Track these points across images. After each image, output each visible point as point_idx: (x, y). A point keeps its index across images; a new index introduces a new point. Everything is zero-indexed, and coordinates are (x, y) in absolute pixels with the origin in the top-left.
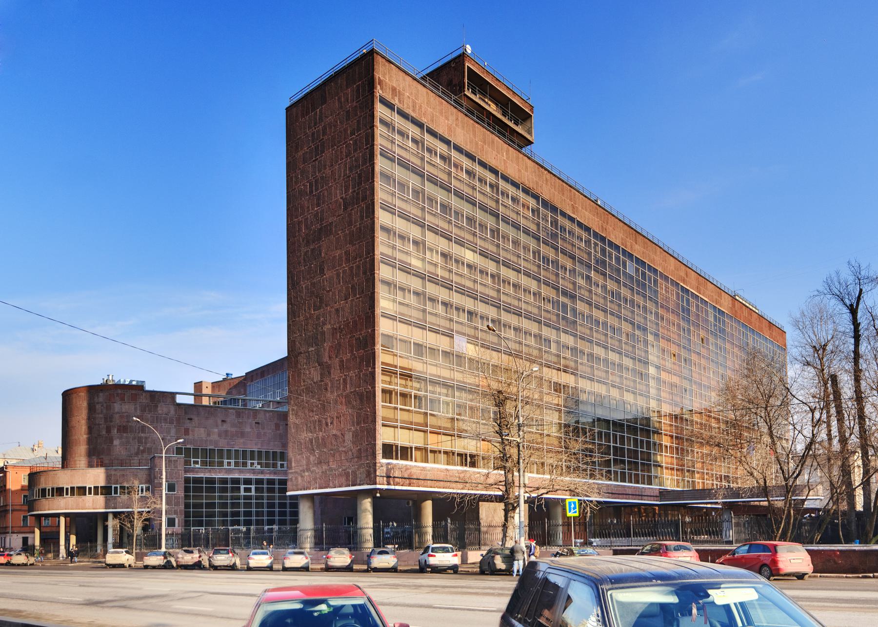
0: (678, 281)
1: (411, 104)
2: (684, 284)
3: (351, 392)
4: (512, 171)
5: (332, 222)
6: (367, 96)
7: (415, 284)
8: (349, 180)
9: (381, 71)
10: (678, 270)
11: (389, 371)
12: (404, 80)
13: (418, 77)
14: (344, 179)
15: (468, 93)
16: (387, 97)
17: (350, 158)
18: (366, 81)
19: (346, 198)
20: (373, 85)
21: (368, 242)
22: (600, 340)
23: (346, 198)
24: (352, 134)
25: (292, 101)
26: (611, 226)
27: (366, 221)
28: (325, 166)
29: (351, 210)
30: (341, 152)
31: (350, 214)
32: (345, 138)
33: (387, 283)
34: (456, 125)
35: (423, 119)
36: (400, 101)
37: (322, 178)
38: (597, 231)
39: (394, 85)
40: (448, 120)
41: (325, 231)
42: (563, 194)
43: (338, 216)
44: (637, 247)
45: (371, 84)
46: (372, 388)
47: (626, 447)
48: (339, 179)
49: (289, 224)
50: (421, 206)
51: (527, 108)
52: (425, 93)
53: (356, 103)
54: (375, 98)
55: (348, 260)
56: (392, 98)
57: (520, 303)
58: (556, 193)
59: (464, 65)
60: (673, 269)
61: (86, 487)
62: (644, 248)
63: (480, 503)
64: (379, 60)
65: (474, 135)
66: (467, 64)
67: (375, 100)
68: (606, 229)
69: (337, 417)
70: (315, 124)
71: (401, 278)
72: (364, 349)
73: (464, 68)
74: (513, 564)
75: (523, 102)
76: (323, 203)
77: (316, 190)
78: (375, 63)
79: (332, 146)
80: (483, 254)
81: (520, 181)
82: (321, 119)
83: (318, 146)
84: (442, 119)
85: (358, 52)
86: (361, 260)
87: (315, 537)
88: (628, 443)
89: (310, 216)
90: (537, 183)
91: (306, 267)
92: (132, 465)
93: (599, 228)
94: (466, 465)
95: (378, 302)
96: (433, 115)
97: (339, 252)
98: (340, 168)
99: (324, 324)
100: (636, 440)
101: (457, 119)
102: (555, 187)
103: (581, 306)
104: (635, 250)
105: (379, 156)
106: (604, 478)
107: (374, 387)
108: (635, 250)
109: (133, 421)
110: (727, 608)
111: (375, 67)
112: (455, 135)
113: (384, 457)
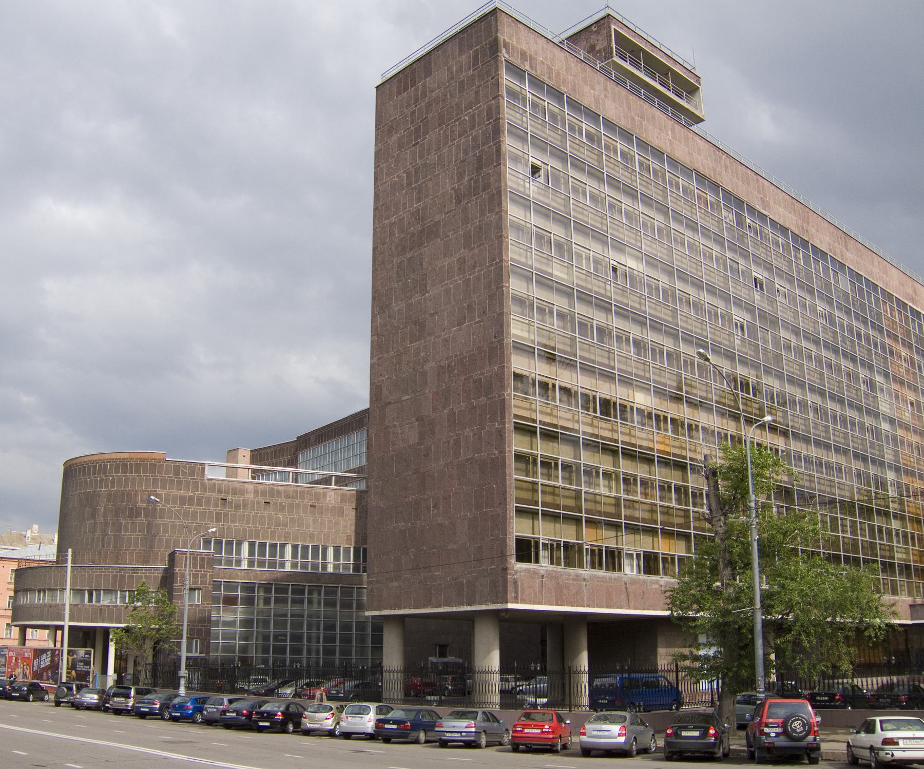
0: (905, 301)
1: (545, 71)
2: (913, 304)
3: (468, 460)
4: (680, 154)
5: (439, 221)
6: (489, 61)
7: (560, 303)
8: (465, 165)
9: (505, 34)
10: (903, 285)
11: (526, 430)
12: (536, 43)
13: (556, 41)
14: (456, 165)
15: (617, 59)
16: (515, 61)
17: (465, 138)
18: (486, 44)
19: (459, 189)
20: (497, 48)
21: (492, 245)
22: (793, 373)
23: (459, 189)
24: (469, 107)
25: (384, 78)
26: (813, 227)
27: (489, 217)
28: (429, 149)
29: (468, 203)
30: (452, 132)
31: (465, 210)
32: (458, 114)
33: (520, 301)
34: (605, 96)
35: (562, 88)
36: (531, 67)
37: (425, 165)
38: (797, 232)
39: (524, 48)
40: (595, 90)
41: (429, 233)
42: (749, 184)
43: (448, 212)
44: (848, 254)
45: (494, 47)
46: (501, 452)
47: (860, 538)
48: (448, 165)
49: (377, 228)
50: (670, 308)
51: (691, 78)
52: (563, 58)
53: (473, 71)
54: (499, 63)
55: (461, 270)
56: (522, 63)
57: (812, 484)
58: (740, 183)
59: (610, 28)
60: (898, 285)
61: (439, 657)
62: (858, 257)
63: (55, 559)
64: (503, 19)
65: (629, 107)
66: (613, 27)
67: (500, 65)
68: (807, 231)
69: (445, 498)
70: (416, 100)
71: (537, 293)
72: (486, 396)
73: (610, 31)
74: (367, 461)
75: (687, 72)
76: (427, 196)
77: (416, 181)
78: (499, 23)
79: (440, 125)
80: (652, 262)
81: (693, 166)
82: (424, 94)
83: (420, 127)
84: (586, 89)
85: (475, 13)
86: (483, 270)
87: (681, 698)
88: (879, 536)
89: (407, 216)
90: (714, 169)
91: (400, 283)
92: (613, 501)
93: (799, 229)
94: (559, 564)
95: (509, 326)
96: (575, 83)
97: (448, 260)
98: (450, 151)
99: (426, 361)
100: (871, 528)
101: (606, 89)
102: (737, 176)
103: (895, 525)
104: (847, 259)
105: (506, 132)
106: (618, 402)
107: (503, 452)
108: (847, 259)
109: (695, 728)
110: (665, 574)
111: (499, 27)
112: (604, 108)
113: (520, 559)
